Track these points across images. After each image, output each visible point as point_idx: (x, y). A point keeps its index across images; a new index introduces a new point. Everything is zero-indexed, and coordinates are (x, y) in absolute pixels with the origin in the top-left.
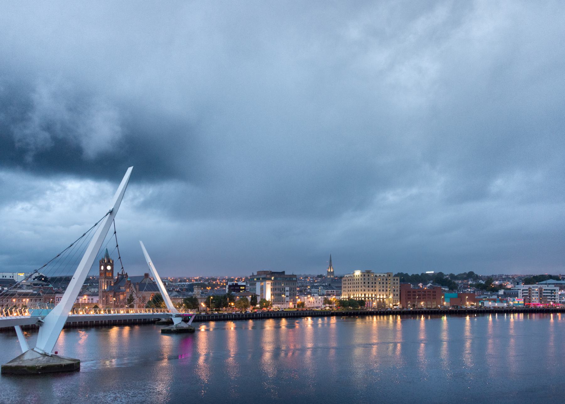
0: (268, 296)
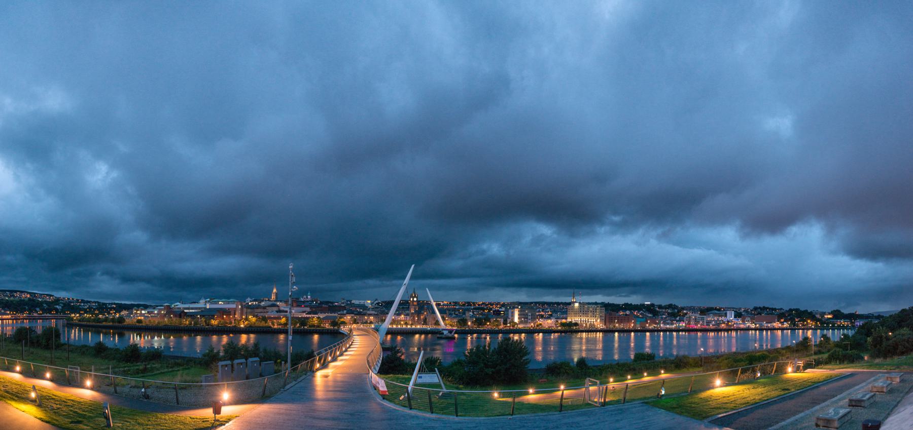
0: (516, 320)
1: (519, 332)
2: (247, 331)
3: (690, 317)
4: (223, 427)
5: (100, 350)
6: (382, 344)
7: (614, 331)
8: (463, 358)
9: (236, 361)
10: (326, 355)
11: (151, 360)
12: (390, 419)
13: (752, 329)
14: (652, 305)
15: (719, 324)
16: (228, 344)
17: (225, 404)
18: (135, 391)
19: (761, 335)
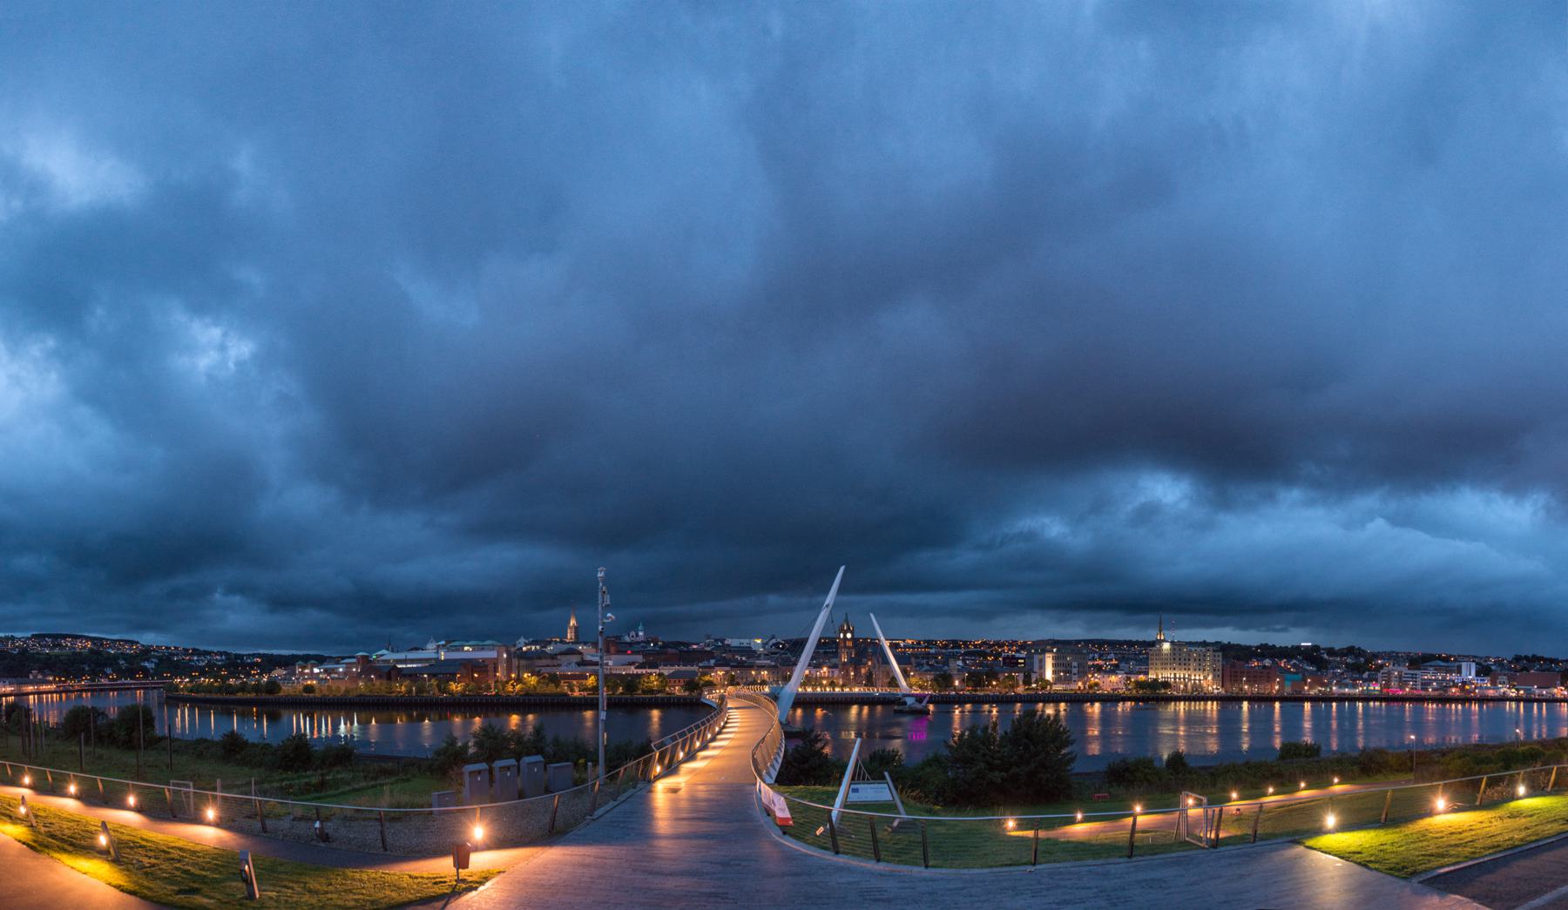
1: (1055, 699)
2: (523, 704)
3: (1389, 673)
4: (474, 893)
5: (233, 748)
6: (786, 725)
7: (1240, 699)
8: (946, 752)
9: (498, 764)
10: (674, 748)
11: (333, 765)
12: (797, 875)
13: (1511, 699)
14: (1315, 648)
15: (1446, 688)
16: (483, 729)
17: (476, 849)
18: (302, 828)
19: (1528, 710)
